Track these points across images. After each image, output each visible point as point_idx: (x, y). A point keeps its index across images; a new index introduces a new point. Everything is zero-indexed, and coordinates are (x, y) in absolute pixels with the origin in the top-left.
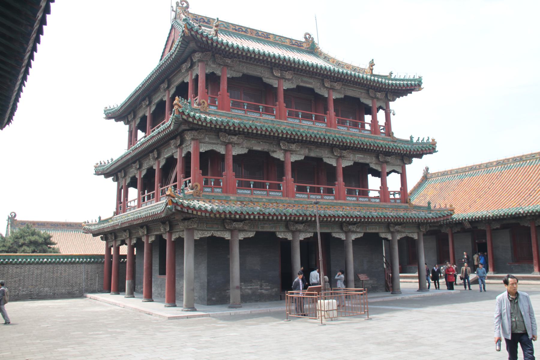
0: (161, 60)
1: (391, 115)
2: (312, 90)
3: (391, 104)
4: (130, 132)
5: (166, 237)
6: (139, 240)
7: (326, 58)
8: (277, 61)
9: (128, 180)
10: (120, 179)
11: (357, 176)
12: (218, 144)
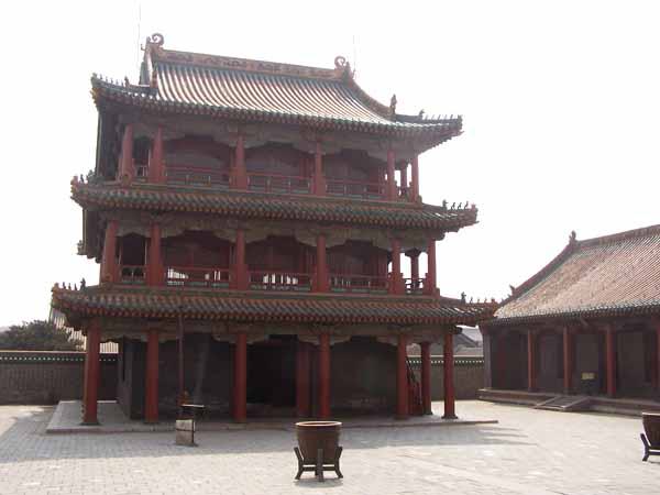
7: (145, 58)
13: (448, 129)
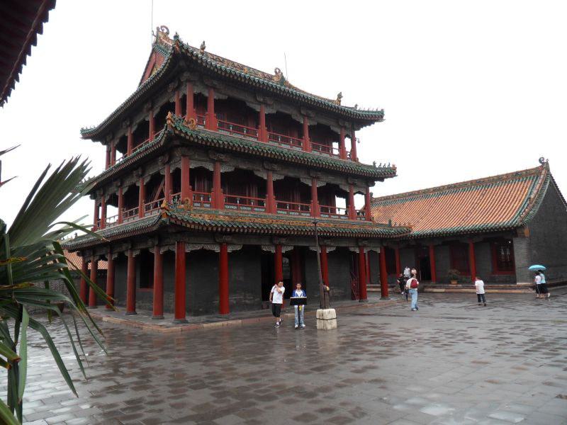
0: (140, 84)
1: (357, 142)
2: (289, 116)
3: (356, 132)
4: (108, 152)
5: (154, 251)
6: (122, 255)
8: (261, 86)
9: (107, 198)
10: (98, 197)
11: (327, 195)
12: (207, 161)
13: (373, 118)
